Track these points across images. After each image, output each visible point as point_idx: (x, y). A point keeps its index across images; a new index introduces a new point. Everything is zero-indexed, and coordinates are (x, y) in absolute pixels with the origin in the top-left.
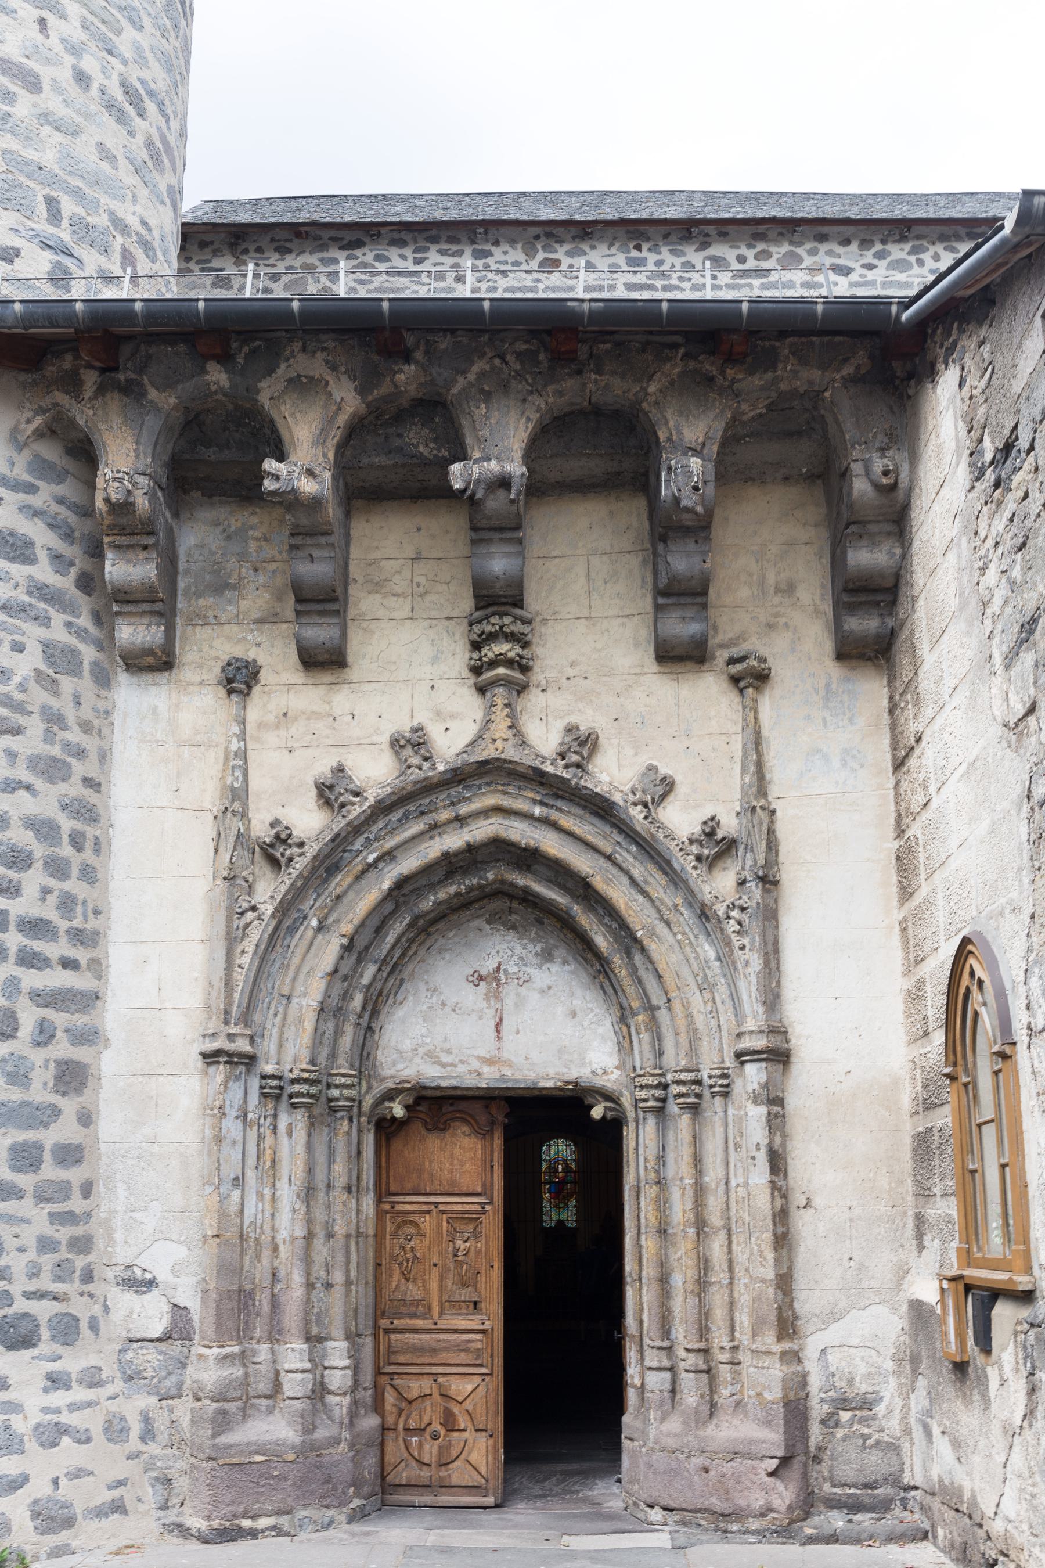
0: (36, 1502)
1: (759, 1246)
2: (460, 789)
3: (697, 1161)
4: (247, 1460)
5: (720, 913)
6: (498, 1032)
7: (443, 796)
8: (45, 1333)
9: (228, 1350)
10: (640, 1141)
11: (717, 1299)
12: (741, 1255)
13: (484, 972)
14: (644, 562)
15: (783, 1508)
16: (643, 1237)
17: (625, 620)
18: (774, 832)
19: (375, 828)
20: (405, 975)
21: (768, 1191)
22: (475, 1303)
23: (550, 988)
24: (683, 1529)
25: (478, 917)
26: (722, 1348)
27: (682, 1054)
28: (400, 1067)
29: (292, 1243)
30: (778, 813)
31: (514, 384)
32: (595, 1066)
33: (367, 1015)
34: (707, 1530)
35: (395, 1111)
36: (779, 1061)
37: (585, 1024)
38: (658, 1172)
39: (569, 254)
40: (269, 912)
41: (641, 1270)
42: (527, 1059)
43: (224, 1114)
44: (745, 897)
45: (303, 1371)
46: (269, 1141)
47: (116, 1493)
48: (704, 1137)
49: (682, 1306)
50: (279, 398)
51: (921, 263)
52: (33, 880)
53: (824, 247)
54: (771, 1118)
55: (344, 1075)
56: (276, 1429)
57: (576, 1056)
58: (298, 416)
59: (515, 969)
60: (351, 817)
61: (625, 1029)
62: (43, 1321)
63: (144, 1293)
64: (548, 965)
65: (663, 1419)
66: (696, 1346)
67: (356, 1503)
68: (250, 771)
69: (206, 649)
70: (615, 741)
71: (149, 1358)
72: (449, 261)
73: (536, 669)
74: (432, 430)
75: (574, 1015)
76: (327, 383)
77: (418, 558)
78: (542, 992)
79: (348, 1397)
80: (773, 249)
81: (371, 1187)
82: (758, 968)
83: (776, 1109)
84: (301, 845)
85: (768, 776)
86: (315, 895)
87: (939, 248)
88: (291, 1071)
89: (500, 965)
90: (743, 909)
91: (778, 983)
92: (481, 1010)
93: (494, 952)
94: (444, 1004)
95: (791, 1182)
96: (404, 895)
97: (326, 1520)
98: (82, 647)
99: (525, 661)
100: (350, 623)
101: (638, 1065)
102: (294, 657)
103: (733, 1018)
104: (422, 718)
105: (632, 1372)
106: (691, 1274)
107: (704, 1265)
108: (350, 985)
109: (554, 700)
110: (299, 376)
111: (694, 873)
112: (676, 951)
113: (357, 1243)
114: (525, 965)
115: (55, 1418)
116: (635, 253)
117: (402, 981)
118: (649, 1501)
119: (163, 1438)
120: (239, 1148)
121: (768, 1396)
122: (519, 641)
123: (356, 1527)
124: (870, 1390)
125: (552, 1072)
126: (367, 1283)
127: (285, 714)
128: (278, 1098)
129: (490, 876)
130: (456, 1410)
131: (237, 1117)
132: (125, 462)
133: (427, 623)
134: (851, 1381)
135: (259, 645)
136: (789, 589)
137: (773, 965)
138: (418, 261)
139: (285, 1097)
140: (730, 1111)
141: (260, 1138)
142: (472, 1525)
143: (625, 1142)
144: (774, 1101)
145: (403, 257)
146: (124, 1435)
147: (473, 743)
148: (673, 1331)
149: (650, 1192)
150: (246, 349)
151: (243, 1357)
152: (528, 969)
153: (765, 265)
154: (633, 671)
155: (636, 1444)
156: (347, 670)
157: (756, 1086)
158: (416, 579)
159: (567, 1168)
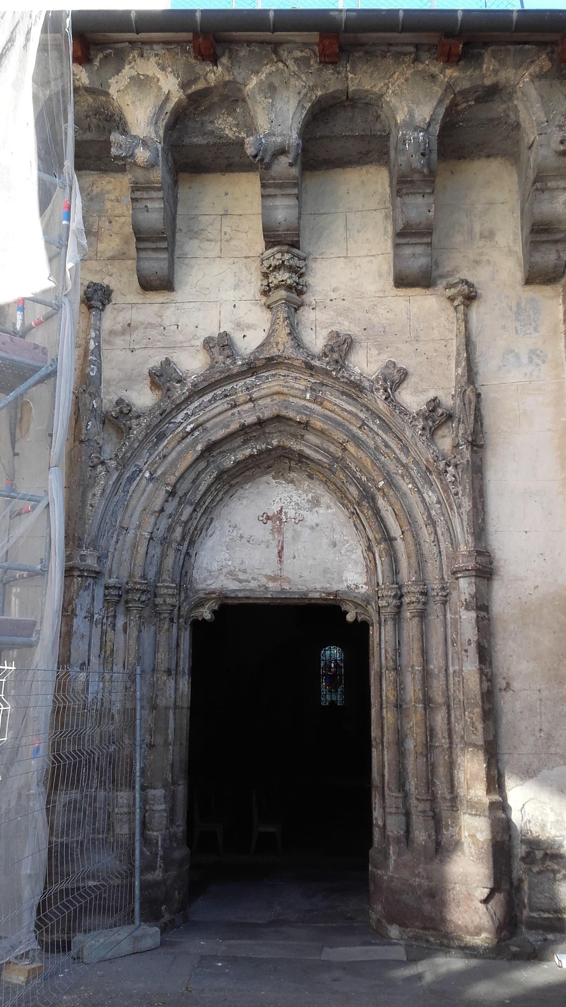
1: (472, 718)
2: (253, 379)
3: (424, 652)
6: (280, 557)
7: (241, 383)
10: (381, 638)
13: (270, 514)
14: (386, 217)
16: (384, 711)
17: (372, 258)
18: (479, 410)
19: (192, 407)
20: (214, 515)
23: (317, 525)
25: (267, 474)
27: (413, 572)
28: (209, 582)
30: (482, 396)
31: (292, 81)
32: (350, 583)
33: (186, 544)
35: (205, 614)
36: (484, 578)
37: (343, 551)
38: (395, 661)
41: (383, 736)
42: (301, 577)
44: (459, 457)
46: (110, 634)
49: (413, 765)
50: (124, 90)
55: (167, 587)
57: (336, 574)
58: (138, 103)
61: (371, 555)
64: (316, 509)
66: (424, 797)
67: (167, 917)
68: (103, 365)
74: (235, 118)
75: (335, 545)
76: (158, 80)
78: (312, 528)
81: (186, 671)
82: (468, 509)
83: (483, 613)
84: (138, 417)
85: (475, 370)
88: (127, 583)
89: (282, 508)
91: (483, 520)
92: (268, 541)
93: (278, 499)
94: (241, 537)
95: (495, 670)
96: (213, 456)
99: (300, 287)
101: (381, 582)
103: (450, 545)
104: (226, 327)
105: (377, 814)
106: (420, 739)
107: (430, 732)
108: (173, 521)
110: (138, 74)
113: (175, 713)
117: (212, 520)
120: (86, 640)
122: (296, 273)
124: (558, 834)
125: (318, 586)
126: (181, 744)
127: (129, 325)
128: (118, 602)
129: (275, 442)
131: (86, 617)
133: (231, 261)
134: (543, 827)
135: (111, 275)
139: (122, 602)
140: (449, 616)
141: (104, 633)
143: (371, 639)
144: (482, 606)
147: (263, 345)
148: (407, 784)
149: (389, 676)
150: (101, 56)
152: (302, 512)
156: (173, 293)
157: (467, 596)
158: (224, 229)
159: (337, 666)
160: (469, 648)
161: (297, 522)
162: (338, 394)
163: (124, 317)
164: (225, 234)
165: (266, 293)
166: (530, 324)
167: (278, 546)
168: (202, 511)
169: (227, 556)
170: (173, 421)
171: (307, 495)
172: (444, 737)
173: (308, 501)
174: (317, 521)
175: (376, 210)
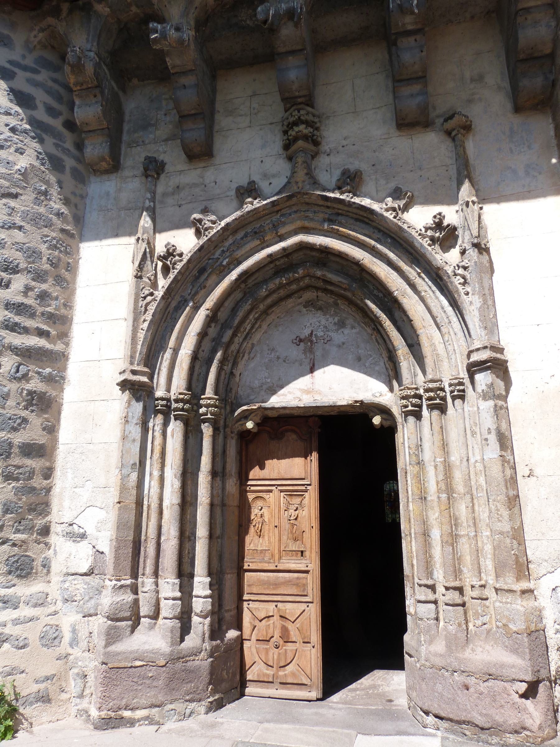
3: (445, 446)
4: (129, 665)
5: (449, 272)
9: (123, 582)
10: (405, 436)
11: (465, 547)
12: (483, 513)
13: (302, 337)
15: (535, 728)
21: (499, 463)
22: (302, 552)
23: (343, 344)
24: (452, 737)
26: (473, 587)
29: (171, 508)
34: (471, 739)
37: (367, 364)
40: (160, 296)
42: (330, 389)
43: (127, 421)
45: (174, 599)
47: (42, 686)
48: (449, 428)
52: (19, 282)
54: (497, 410)
55: (209, 398)
56: (153, 640)
58: (172, 3)
59: (322, 334)
60: (210, 235)
63: (79, 542)
64: (342, 330)
65: (431, 642)
66: (453, 584)
69: (134, 158)
70: (373, 177)
71: (78, 586)
73: (323, 143)
77: (254, 94)
78: (339, 346)
79: (209, 619)
82: (479, 305)
83: (500, 403)
84: (181, 255)
86: (191, 287)
90: (465, 268)
93: (308, 325)
97: (188, 712)
98: (65, 157)
100: (215, 134)
102: (184, 156)
109: (336, 159)
111: (429, 248)
112: (420, 303)
114: (328, 331)
118: (425, 708)
119: (84, 644)
127: (178, 187)
130: (290, 626)
131: (136, 424)
136: (480, 78)
137: (490, 303)
146: (56, 642)
148: (435, 573)
149: (412, 470)
151: (135, 590)
152: (330, 334)
154: (383, 137)
155: (413, 659)
157: (484, 387)
160: (489, 437)
161: (325, 342)
162: (352, 221)
163: (175, 181)
164: (254, 109)
165: (286, 147)
166: (524, 144)
167: (310, 364)
168: (243, 336)
169: (267, 374)
170: (211, 257)
171: (334, 319)
172: (469, 526)
173: (335, 324)
174: (342, 340)
175: (377, 73)
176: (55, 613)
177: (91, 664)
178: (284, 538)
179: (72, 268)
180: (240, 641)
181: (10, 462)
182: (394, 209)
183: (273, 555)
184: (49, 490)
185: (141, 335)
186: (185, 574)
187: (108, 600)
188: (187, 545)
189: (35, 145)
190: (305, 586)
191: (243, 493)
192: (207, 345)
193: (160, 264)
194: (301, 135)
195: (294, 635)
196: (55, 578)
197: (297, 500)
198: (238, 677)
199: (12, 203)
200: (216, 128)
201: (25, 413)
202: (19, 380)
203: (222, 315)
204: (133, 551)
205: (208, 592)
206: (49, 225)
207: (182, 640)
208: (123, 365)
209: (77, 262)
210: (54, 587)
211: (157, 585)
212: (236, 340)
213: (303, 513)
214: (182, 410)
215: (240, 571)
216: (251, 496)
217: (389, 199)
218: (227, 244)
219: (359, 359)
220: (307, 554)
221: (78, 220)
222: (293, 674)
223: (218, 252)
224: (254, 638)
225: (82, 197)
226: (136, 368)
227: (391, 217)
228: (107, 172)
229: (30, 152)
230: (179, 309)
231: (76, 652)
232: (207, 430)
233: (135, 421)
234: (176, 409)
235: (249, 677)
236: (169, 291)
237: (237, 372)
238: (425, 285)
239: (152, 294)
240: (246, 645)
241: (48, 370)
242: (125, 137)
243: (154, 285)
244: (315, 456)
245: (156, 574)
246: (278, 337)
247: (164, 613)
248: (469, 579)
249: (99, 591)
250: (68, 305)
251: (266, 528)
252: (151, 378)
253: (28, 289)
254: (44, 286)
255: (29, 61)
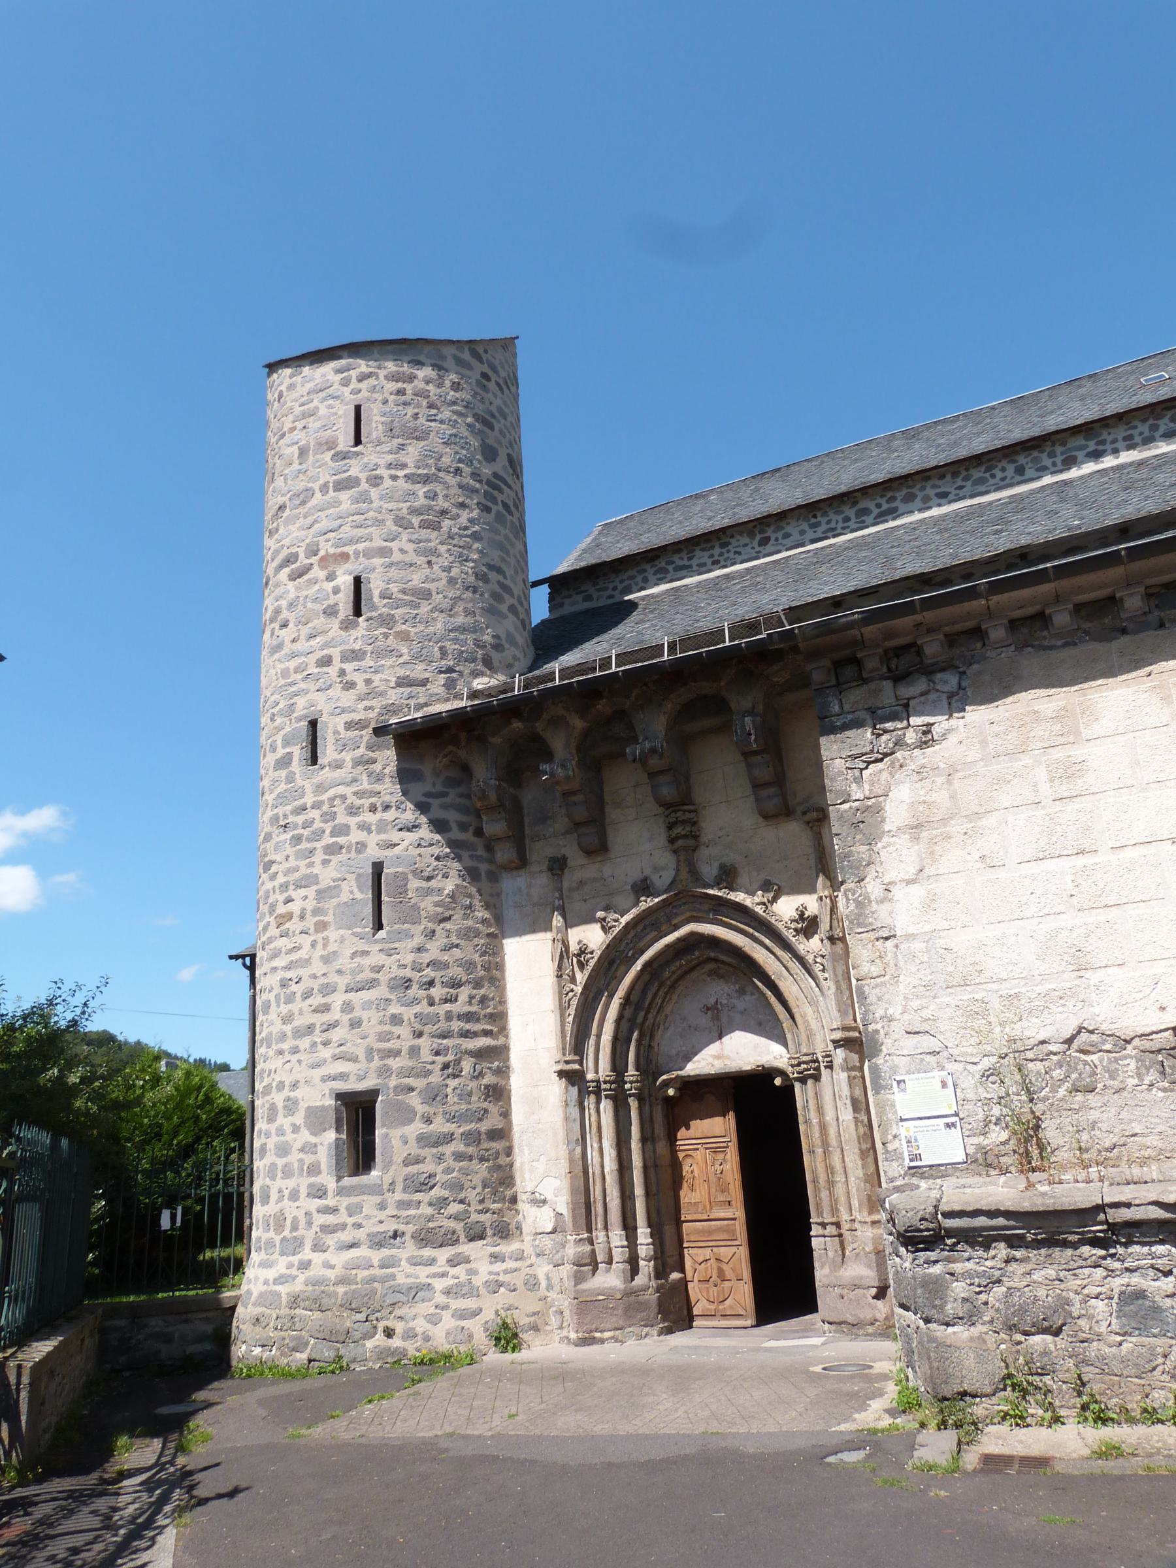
0: (486, 1322)
8: (489, 1232)
11: (840, 1190)
12: (849, 1164)
39: (774, 532)
51: (993, 476)
52: (464, 993)
53: (929, 484)
62: (488, 1224)
69: (541, 852)
72: (707, 554)
78: (742, 1013)
80: (897, 494)
84: (592, 953)
87: (1004, 463)
90: (823, 957)
109: (714, 851)
115: (496, 1277)
116: (813, 520)
117: (666, 1016)
121: (867, 1249)
123: (662, 1337)
130: (725, 1267)
132: (483, 772)
138: (690, 559)
142: (726, 1336)
145: (682, 559)
151: (591, 1241)
153: (893, 505)
176: (532, 1265)
177: (565, 1303)
178: (713, 1190)
179: (500, 967)
180: (684, 1282)
181: (481, 1147)
182: (764, 904)
183: (705, 1207)
184: (511, 1165)
185: (568, 1028)
186: (629, 1227)
187: (571, 1251)
188: (629, 1203)
189: (457, 865)
190: (734, 1231)
191: (674, 1152)
192: (625, 1025)
193: (575, 960)
194: (681, 821)
195: (729, 1274)
196: (527, 1238)
197: (721, 1156)
198: (685, 1312)
199: (448, 925)
200: (607, 821)
201: (485, 1105)
202: (476, 1078)
203: (634, 998)
204: (585, 1211)
205: (650, 1240)
206: (477, 934)
207: (633, 1279)
208: (558, 1056)
209: (503, 958)
210: (526, 1244)
211: (608, 1236)
212: (650, 1016)
213: (727, 1167)
214: (610, 1090)
215: (678, 1223)
216: (681, 1155)
217: (760, 893)
218: (629, 937)
219: (760, 1024)
220: (733, 1203)
221: (498, 919)
222: (731, 1307)
223: (624, 944)
224: (696, 1279)
225: (498, 895)
226: (568, 1058)
227: (761, 912)
228: (518, 868)
229: (453, 873)
230: (596, 999)
231: (552, 1295)
232: (633, 1104)
233: (573, 1103)
234: (605, 1090)
235: (695, 1313)
236: (586, 987)
237: (654, 1044)
238: (795, 966)
239: (572, 991)
240: (690, 1285)
241: (496, 1063)
242: (527, 831)
243: (573, 980)
244: (731, 1115)
245: (606, 1228)
246: (687, 1008)
247: (615, 1259)
248: (845, 1216)
249: (563, 1245)
250: (503, 1002)
251: (697, 1182)
252: (581, 1064)
253: (471, 997)
254: (482, 991)
255: (439, 788)
